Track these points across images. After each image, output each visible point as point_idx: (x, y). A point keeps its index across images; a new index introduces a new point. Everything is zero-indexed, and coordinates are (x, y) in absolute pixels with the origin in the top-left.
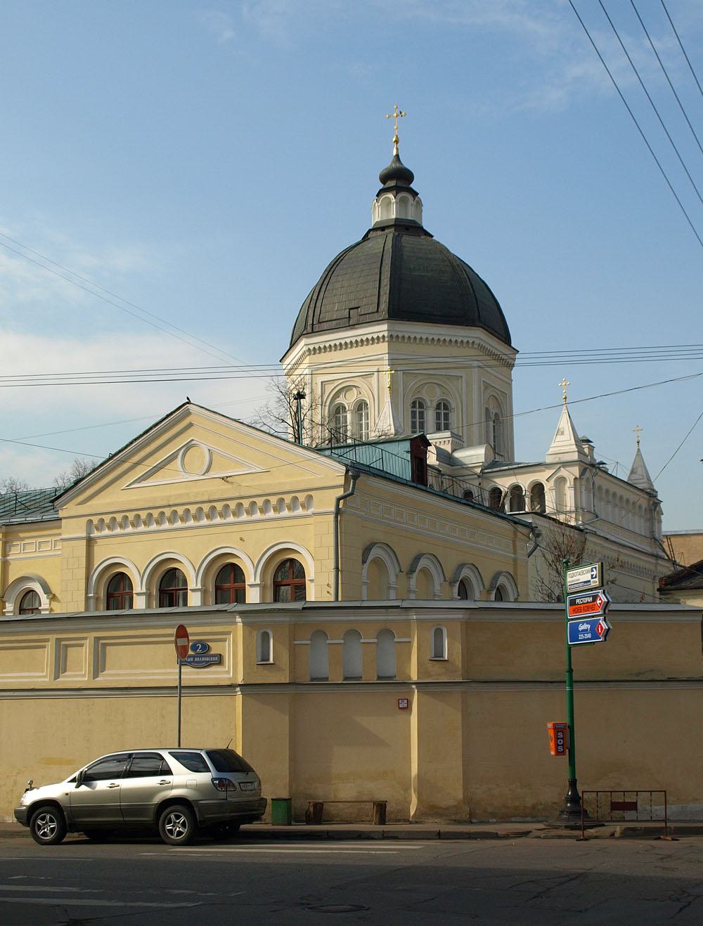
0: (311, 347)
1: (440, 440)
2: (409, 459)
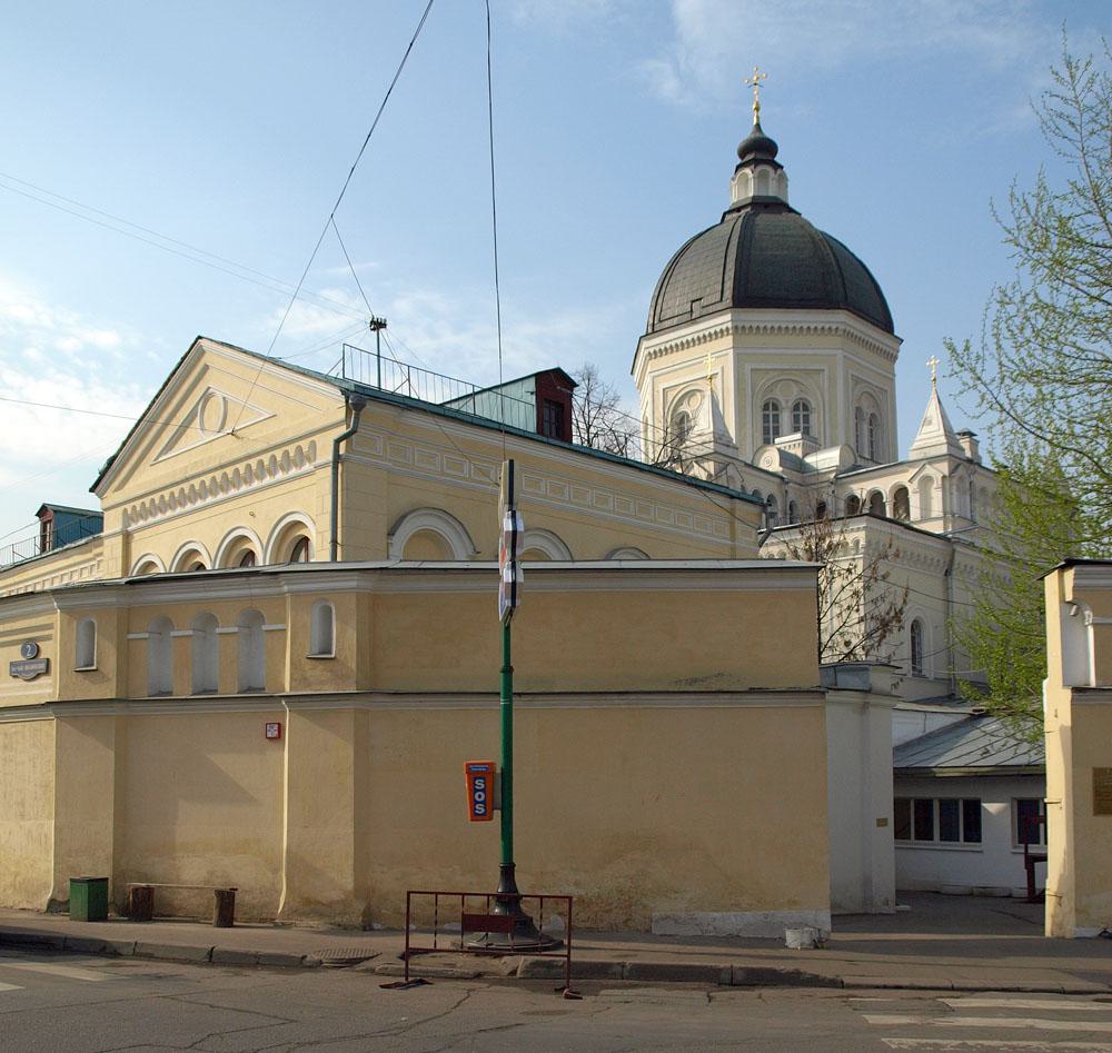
0: (652, 350)
2: (534, 403)
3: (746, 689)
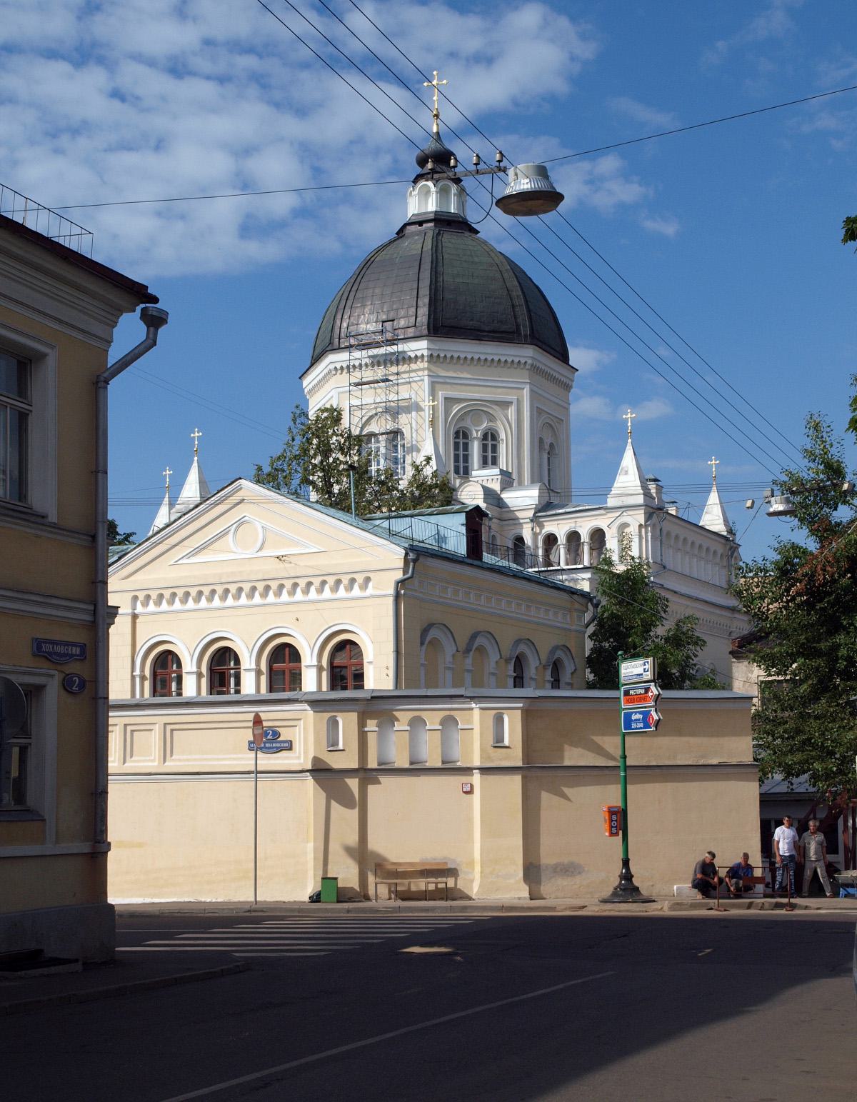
2: (464, 532)
3: (626, 754)
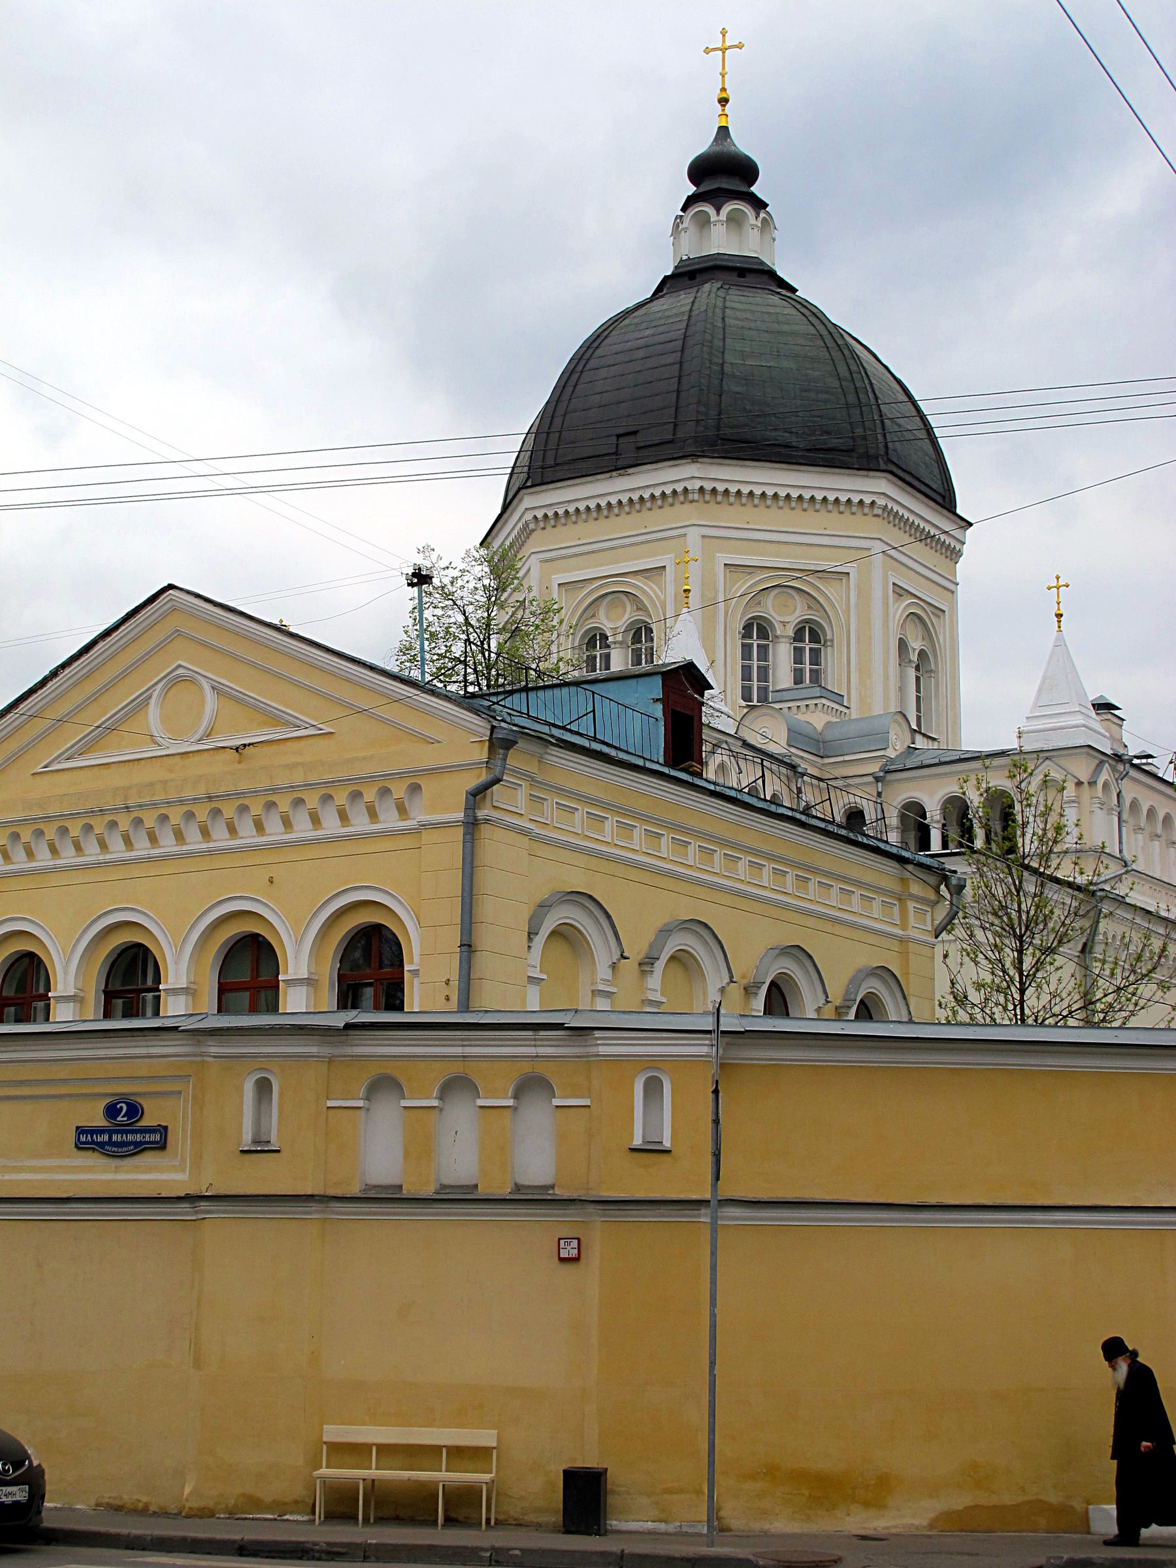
1: (808, 702)
